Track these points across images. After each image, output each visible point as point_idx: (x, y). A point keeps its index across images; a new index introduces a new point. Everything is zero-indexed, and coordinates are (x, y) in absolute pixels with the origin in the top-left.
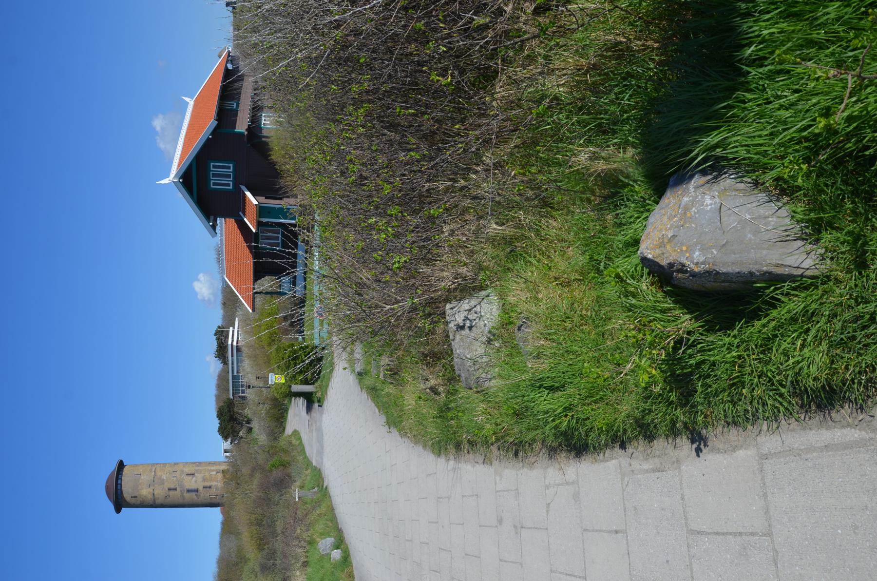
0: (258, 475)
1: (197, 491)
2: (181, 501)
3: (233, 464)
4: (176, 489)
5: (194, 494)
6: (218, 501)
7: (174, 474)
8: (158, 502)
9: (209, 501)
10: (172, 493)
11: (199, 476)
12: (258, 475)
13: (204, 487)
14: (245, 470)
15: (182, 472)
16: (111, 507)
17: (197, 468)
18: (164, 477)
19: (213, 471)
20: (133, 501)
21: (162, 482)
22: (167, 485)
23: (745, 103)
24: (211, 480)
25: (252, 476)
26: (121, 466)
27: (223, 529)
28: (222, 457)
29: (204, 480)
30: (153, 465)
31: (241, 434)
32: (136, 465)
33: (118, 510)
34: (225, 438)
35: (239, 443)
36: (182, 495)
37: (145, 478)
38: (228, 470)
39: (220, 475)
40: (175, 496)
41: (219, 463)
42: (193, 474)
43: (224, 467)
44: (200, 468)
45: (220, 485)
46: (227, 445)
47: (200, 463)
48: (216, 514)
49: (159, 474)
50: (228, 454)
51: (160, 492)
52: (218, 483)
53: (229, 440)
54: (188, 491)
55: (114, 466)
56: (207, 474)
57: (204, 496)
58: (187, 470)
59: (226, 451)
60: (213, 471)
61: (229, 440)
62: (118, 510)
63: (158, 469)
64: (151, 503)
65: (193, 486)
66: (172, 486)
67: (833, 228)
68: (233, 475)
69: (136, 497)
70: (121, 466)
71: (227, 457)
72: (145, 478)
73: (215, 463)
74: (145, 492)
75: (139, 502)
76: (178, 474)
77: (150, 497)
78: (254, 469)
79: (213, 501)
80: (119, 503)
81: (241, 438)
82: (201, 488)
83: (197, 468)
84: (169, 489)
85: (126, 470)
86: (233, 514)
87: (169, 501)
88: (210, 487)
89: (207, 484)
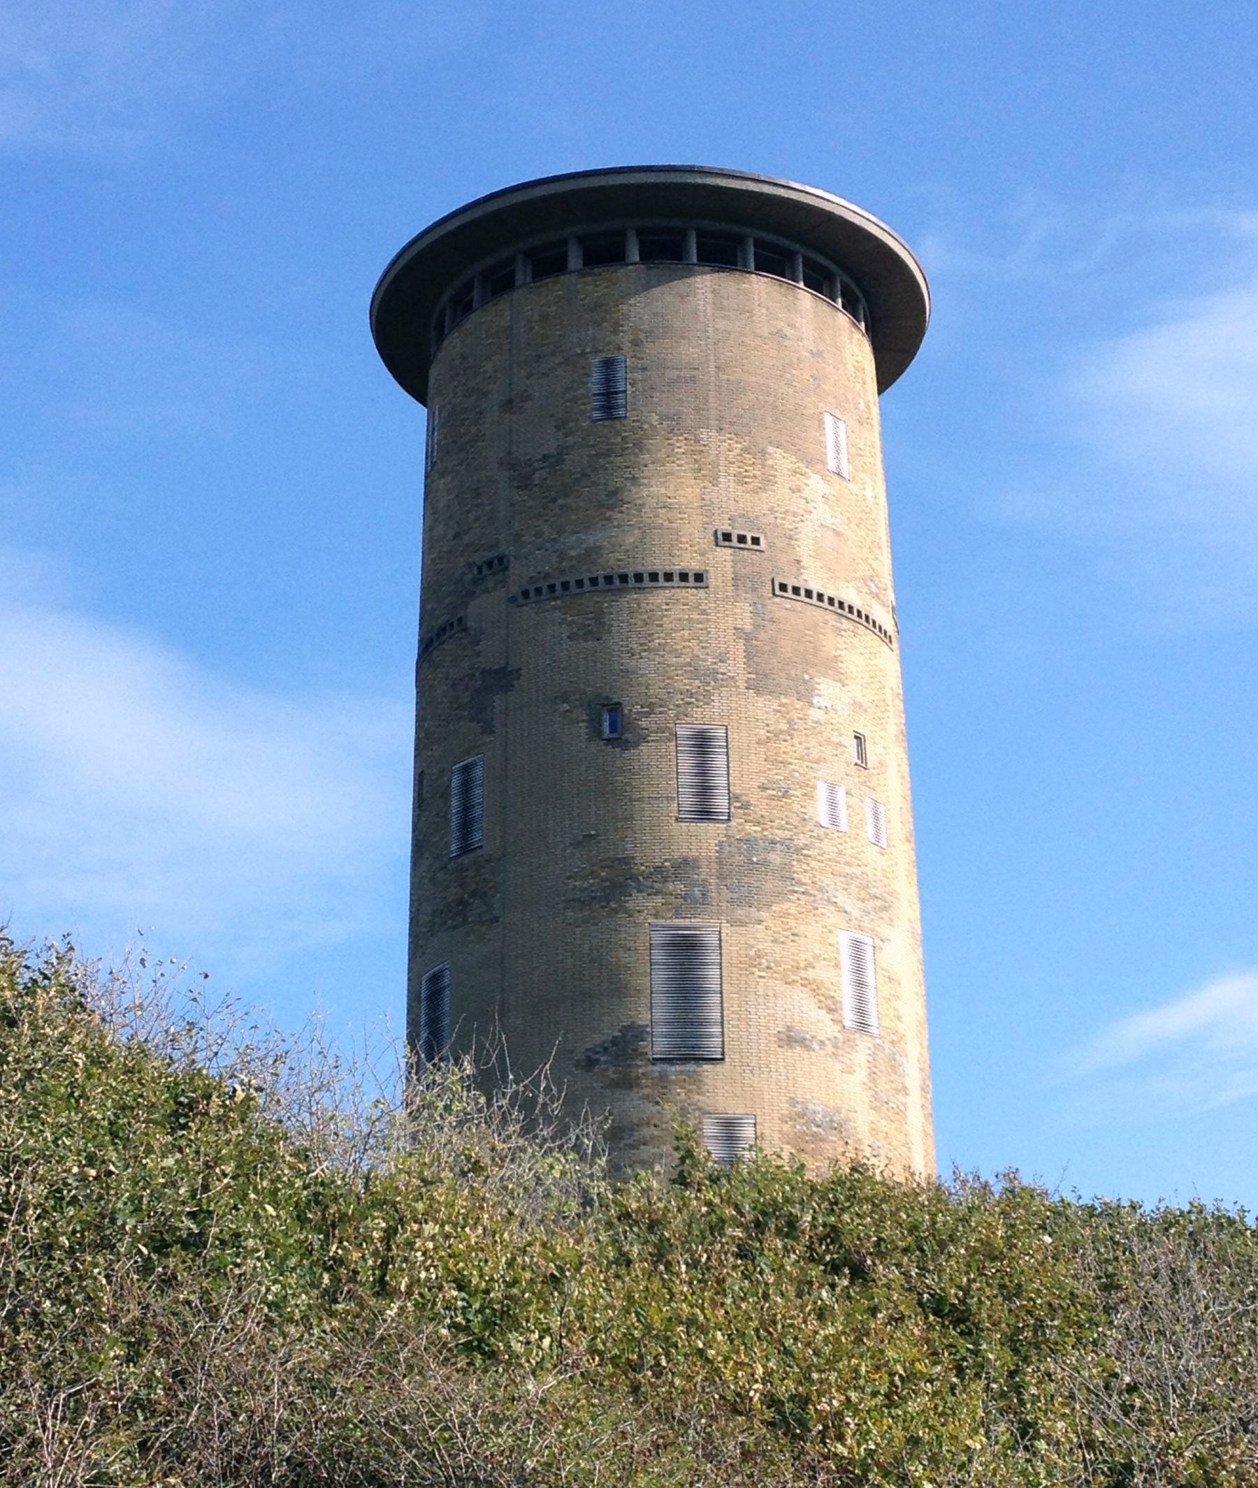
4: (705, 813)
67: (614, 1042)
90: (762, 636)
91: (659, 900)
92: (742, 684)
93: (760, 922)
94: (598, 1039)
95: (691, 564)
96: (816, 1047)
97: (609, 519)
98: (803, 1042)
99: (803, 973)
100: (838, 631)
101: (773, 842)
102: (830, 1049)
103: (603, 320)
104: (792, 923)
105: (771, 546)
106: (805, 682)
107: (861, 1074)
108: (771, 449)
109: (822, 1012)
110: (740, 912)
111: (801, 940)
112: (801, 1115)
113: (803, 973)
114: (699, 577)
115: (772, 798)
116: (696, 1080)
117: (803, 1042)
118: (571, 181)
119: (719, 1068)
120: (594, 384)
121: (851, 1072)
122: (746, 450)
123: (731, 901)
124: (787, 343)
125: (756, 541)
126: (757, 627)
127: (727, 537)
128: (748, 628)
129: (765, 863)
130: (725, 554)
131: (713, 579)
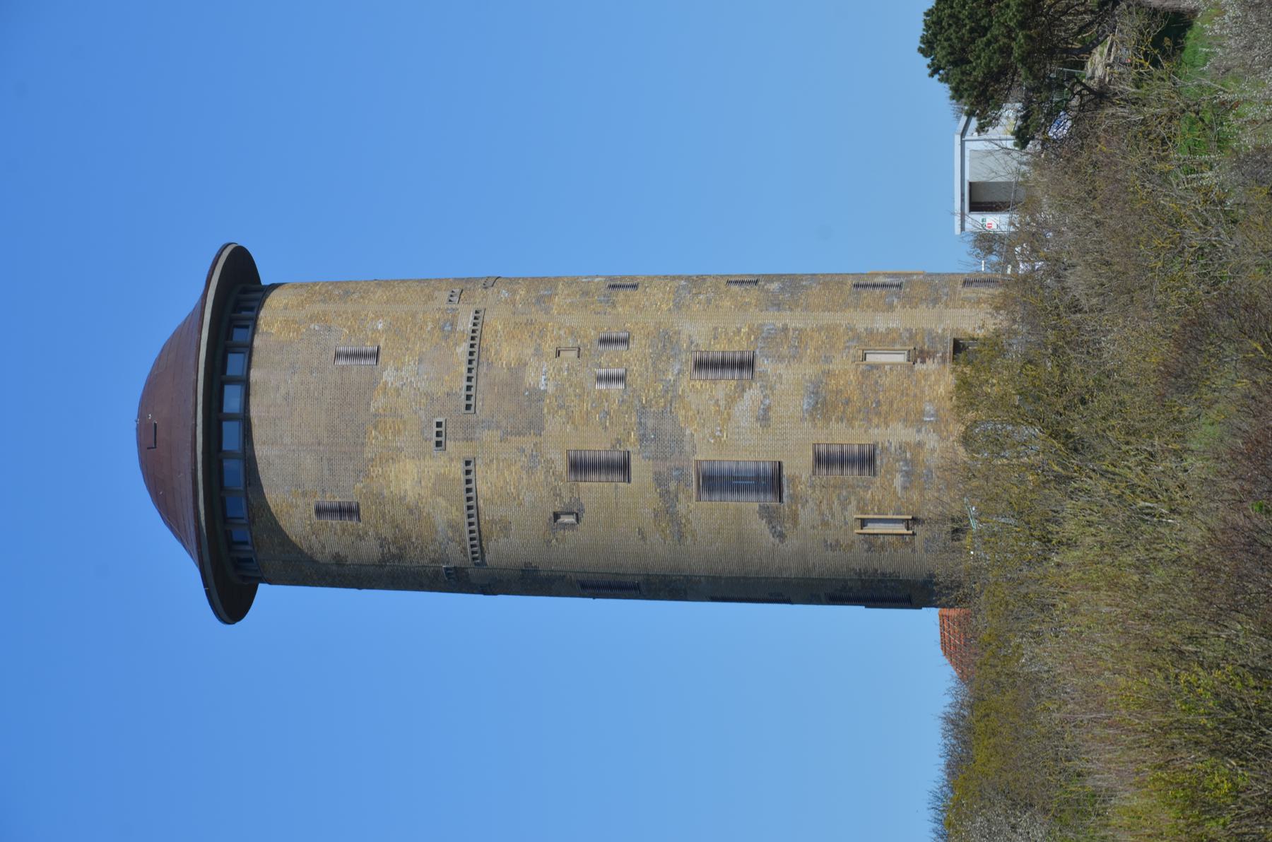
0: (1231, 381)
1: (771, 482)
2: (659, 552)
3: (1044, 305)
4: (622, 467)
5: (750, 505)
6: (923, 558)
7: (611, 361)
8: (503, 550)
9: (859, 559)
10: (595, 489)
11: (786, 378)
12: (1231, 381)
13: (824, 460)
14: (1131, 344)
15: (666, 342)
16: (181, 573)
17: (773, 319)
18: (540, 377)
19: (887, 341)
20: (330, 539)
21: (528, 414)
22: (563, 437)
23: (288, 394)
24: (874, 411)
25: (1181, 379)
26: (239, 288)
27: (959, 767)
28: (949, 241)
29: (822, 404)
30: (461, 288)
31: (1097, 65)
32: (344, 290)
33: (231, 600)
34: (979, 99)
35: (1081, 136)
36: (668, 513)
37: (415, 376)
38: (995, 345)
39: (939, 380)
40: (621, 515)
41: (933, 289)
42: (745, 365)
43: (974, 320)
44: (793, 320)
45: (938, 445)
46: (991, 150)
47: (792, 283)
48: (904, 663)
49: (504, 352)
50: (996, 222)
51: (515, 489)
52: (922, 430)
53: (1010, 115)
54: (715, 482)
55: (187, 291)
56: (843, 365)
57: (826, 520)
58: (701, 331)
59: (980, 199)
60: (887, 341)
61: (1010, 115)
62: (231, 600)
63: (495, 322)
64: (457, 556)
65: (746, 449)
66: (598, 445)
67: (770, 522)
68: (1038, 385)
69: (348, 511)
70: (239, 288)
71: (986, 241)
72: (415, 376)
73: (895, 288)
74: (412, 483)
75: (370, 550)
76: (632, 358)
77: (445, 513)
78: (1195, 334)
79: (886, 563)
80: (238, 554)
81: (1101, 96)
82: (798, 466)
83: (773, 319)
84: (580, 466)
85: (273, 318)
86: (1041, 656)
87: (575, 546)
88: (866, 460)
89: (846, 436)
90: (504, 423)
91: (681, 496)
92: (538, 439)
93: (692, 435)
94: (767, 531)
95: (458, 469)
96: (767, 402)
97: (429, 514)
98: (767, 410)
99: (722, 409)
100: (490, 365)
101: (640, 423)
102: (768, 392)
103: (288, 512)
104: (691, 413)
105: (440, 414)
106: (530, 394)
107: (781, 368)
108: (372, 410)
109: (746, 395)
110: (688, 448)
111: (701, 408)
112: (811, 415)
113: (722, 409)
114: (468, 463)
115: (611, 423)
116: (792, 479)
117: (767, 410)
118: (191, 486)
119: (785, 465)
120: (335, 522)
121: (780, 376)
122: (375, 428)
123: (681, 453)
124: (292, 393)
125: (439, 425)
126: (498, 427)
127: (438, 444)
128: (499, 433)
129: (654, 430)
130: (450, 445)
131: (468, 455)
